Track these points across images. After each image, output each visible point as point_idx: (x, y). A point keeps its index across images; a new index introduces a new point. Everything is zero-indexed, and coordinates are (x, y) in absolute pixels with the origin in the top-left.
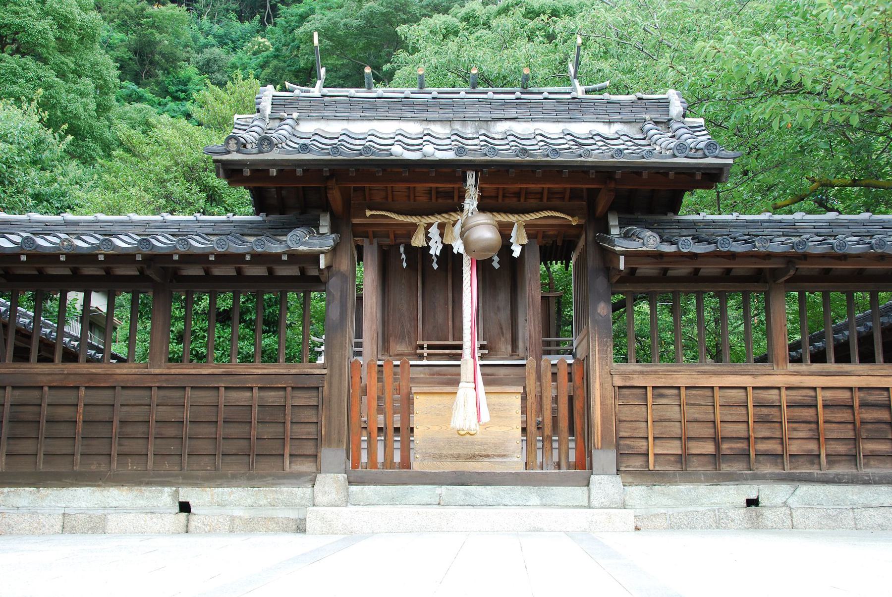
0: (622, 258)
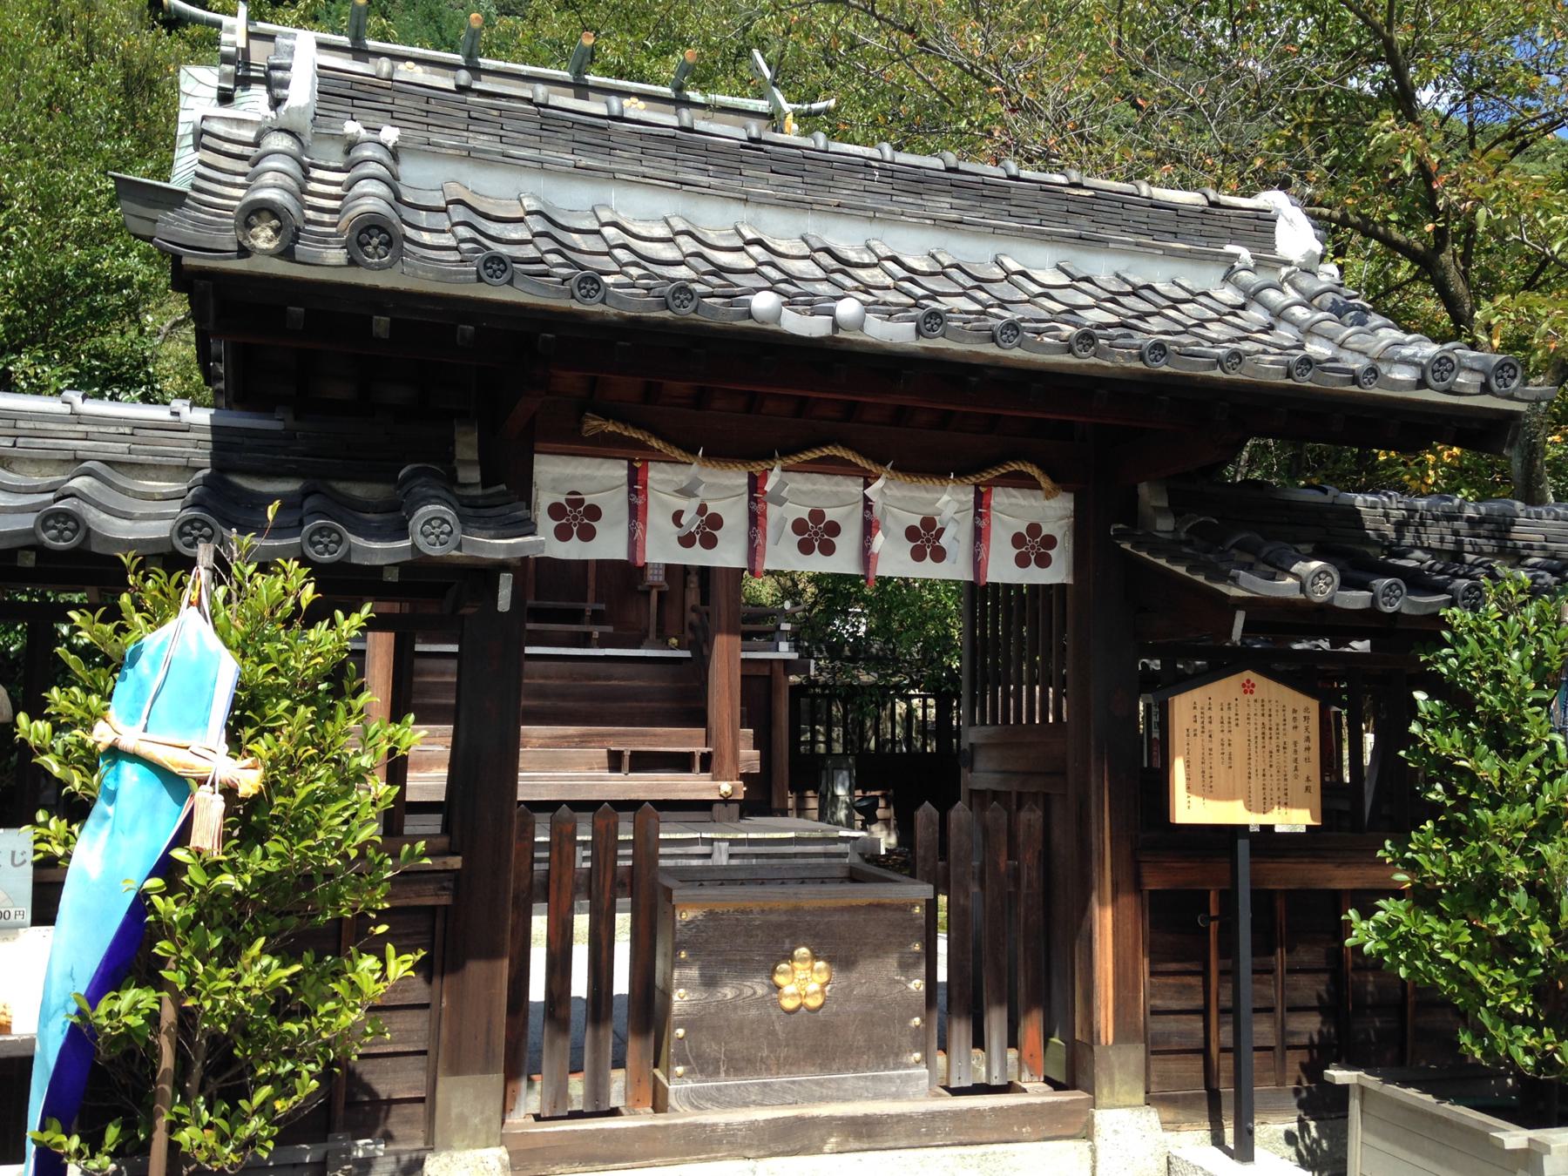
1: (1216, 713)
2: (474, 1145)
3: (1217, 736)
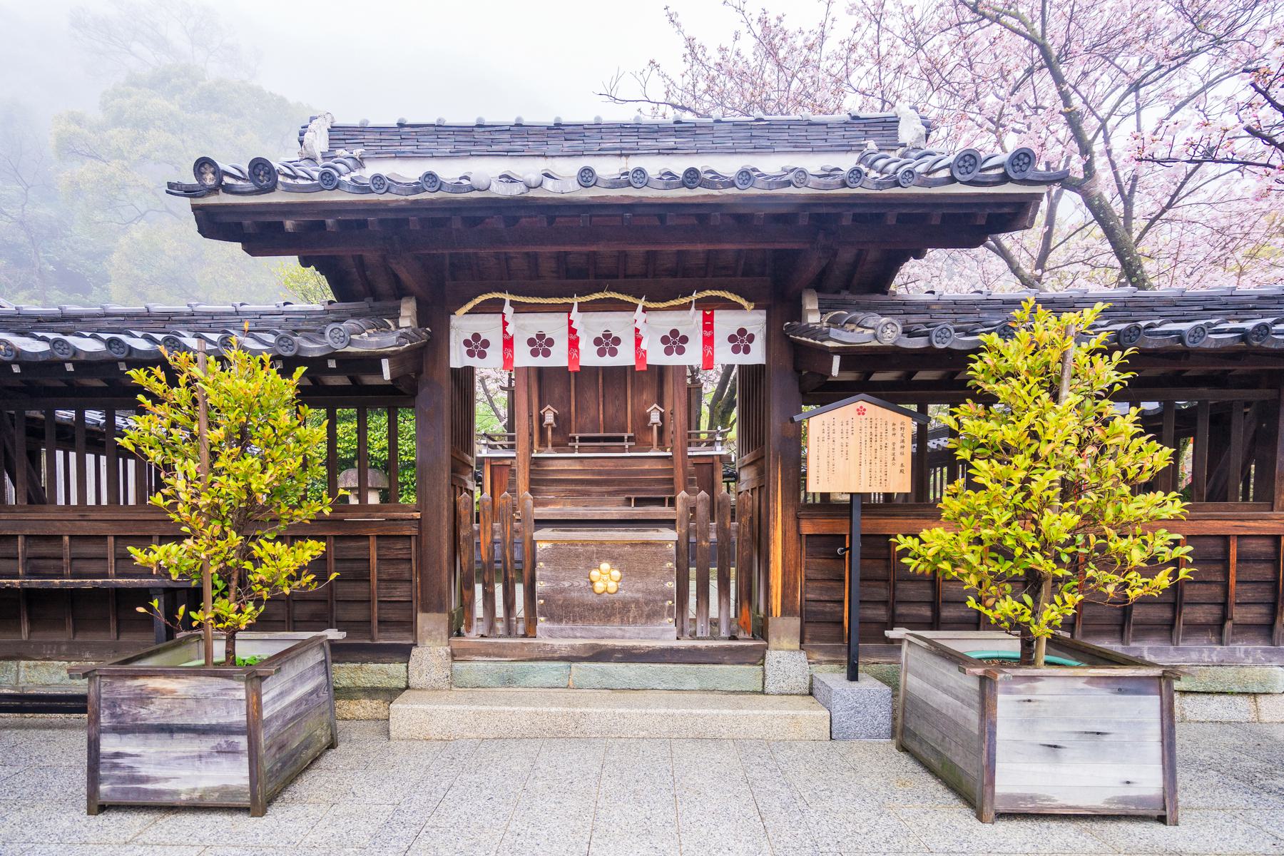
0: (836, 360)
1: (838, 428)
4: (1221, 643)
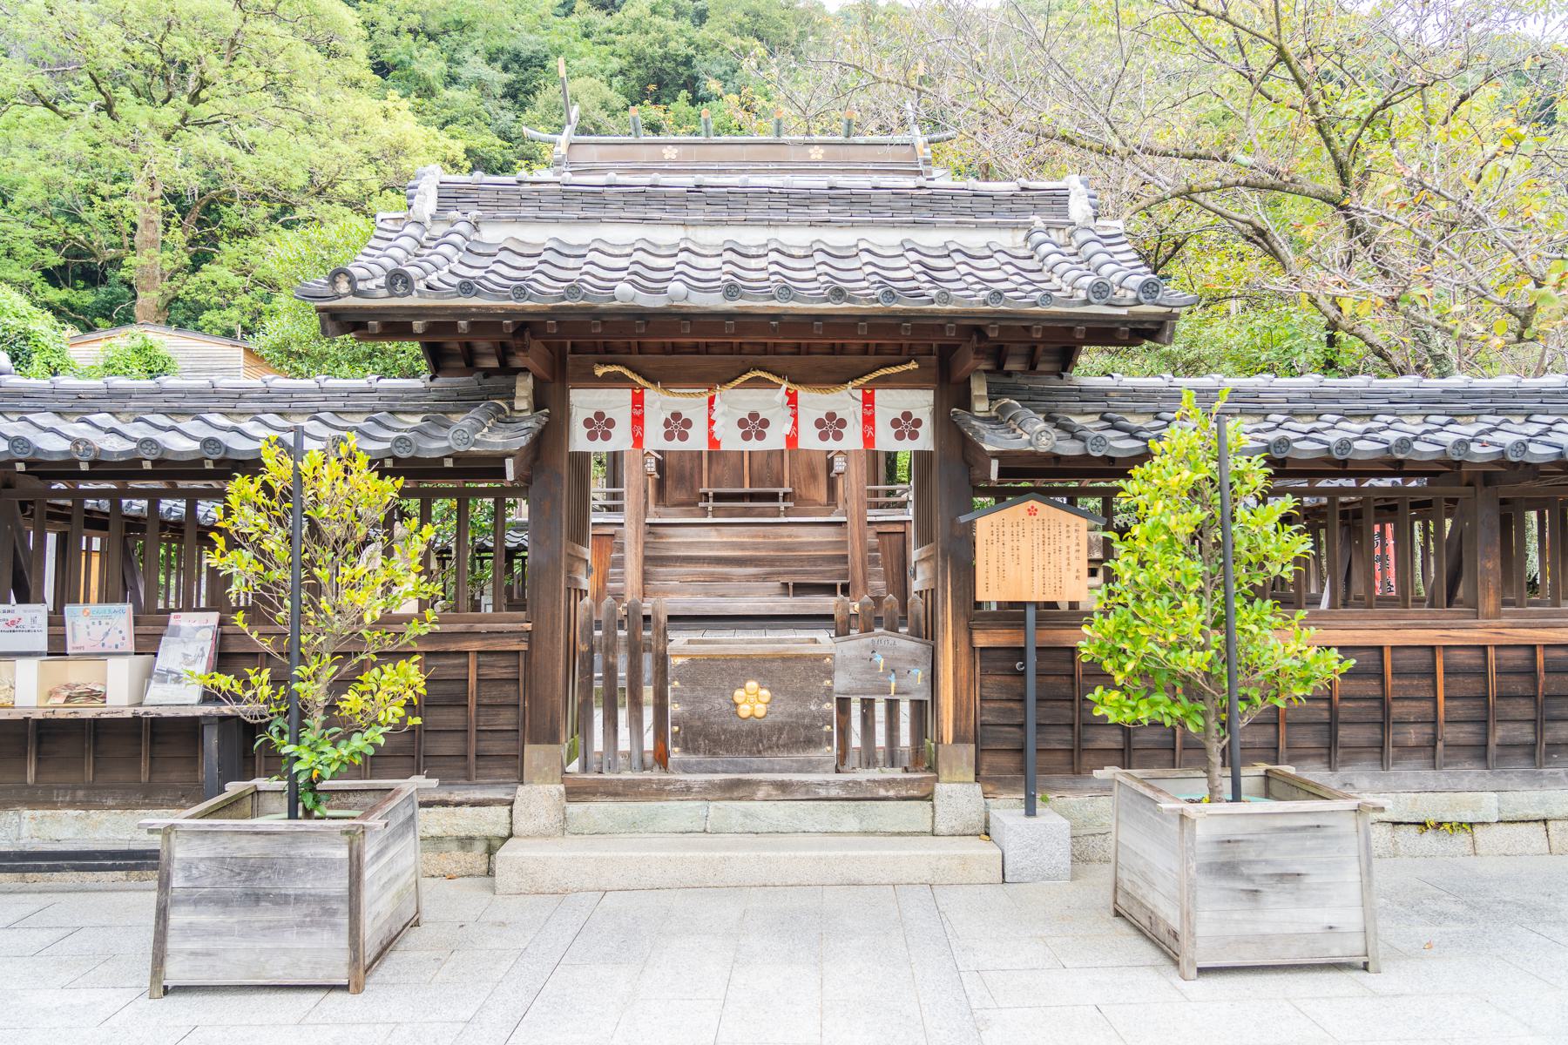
1: (1008, 529)
2: (545, 781)
3: (1008, 546)
4: (1434, 767)
